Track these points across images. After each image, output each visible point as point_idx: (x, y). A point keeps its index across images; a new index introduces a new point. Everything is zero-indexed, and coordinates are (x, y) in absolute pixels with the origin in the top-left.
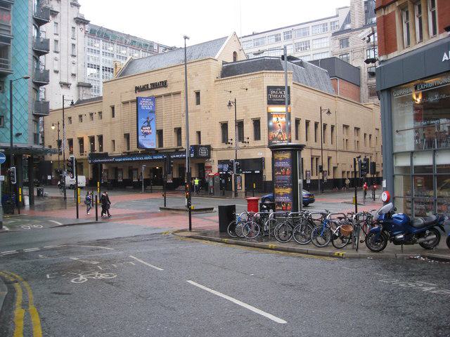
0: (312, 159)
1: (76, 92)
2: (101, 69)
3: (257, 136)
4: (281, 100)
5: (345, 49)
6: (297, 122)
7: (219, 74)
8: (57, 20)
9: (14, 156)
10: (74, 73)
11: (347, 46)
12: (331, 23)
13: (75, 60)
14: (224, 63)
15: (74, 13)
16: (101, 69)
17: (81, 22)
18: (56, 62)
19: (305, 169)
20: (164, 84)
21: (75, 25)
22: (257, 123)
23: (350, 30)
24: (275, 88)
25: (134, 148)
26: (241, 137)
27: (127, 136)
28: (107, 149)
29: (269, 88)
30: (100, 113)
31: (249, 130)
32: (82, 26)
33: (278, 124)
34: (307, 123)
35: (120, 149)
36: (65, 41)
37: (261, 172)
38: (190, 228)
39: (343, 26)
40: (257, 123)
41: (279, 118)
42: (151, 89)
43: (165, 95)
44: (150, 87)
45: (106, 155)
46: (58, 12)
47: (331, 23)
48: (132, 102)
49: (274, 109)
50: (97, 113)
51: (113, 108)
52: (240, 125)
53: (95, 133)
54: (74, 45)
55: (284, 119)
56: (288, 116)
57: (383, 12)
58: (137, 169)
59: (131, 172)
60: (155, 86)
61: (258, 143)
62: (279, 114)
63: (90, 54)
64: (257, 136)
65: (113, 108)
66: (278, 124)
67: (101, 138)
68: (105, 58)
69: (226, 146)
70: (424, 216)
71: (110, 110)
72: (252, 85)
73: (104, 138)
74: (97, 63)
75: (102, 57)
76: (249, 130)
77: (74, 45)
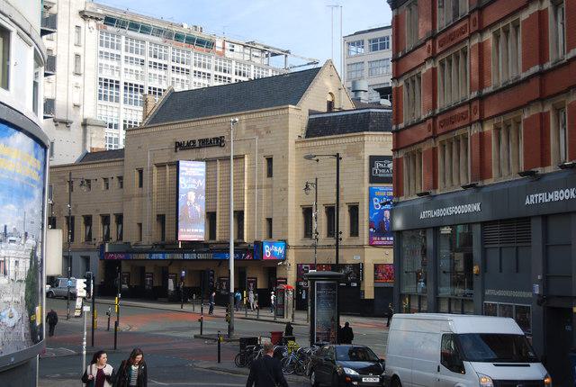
0: (371, 245)
1: (82, 130)
2: (122, 86)
3: (354, 232)
7: (303, 133)
10: (77, 103)
13: (79, 80)
14: (311, 113)
16: (122, 86)
20: (219, 142)
21: (81, 22)
26: (332, 230)
28: (131, 236)
29: (373, 159)
30: (120, 178)
37: (359, 285)
38: (115, 348)
42: (200, 147)
46: (54, 4)
50: (115, 178)
52: (332, 212)
53: (112, 211)
54: (77, 56)
57: (433, 142)
60: (205, 143)
61: (355, 241)
63: (104, 61)
64: (354, 232)
65: (141, 172)
67: (120, 219)
68: (129, 66)
69: (309, 242)
70: (140, 363)
71: (137, 175)
75: (124, 65)
77: (77, 56)
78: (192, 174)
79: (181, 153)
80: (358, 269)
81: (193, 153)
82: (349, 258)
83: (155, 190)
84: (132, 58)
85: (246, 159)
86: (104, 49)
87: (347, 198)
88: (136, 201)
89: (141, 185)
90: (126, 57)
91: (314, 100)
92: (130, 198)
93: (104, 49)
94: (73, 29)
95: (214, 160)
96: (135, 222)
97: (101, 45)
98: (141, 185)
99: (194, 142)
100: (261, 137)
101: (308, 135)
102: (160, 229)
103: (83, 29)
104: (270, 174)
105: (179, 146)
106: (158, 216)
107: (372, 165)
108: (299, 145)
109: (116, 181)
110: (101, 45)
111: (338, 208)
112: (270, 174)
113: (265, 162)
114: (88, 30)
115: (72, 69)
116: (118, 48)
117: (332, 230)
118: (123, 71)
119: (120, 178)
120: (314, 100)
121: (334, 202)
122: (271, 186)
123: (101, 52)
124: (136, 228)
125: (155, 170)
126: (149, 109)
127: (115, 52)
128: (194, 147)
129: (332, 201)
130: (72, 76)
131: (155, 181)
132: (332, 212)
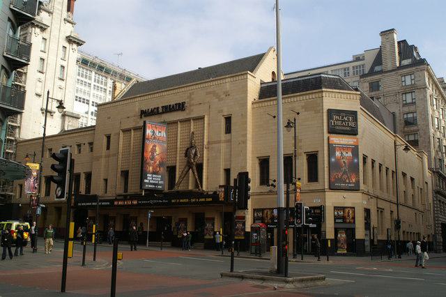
2: (91, 103)
3: (313, 176)
4: (344, 128)
5: (377, 92)
6: (365, 158)
8: (45, 35)
9: (4, 235)
11: (378, 90)
12: (353, 67)
13: (63, 84)
15: (68, 30)
16: (91, 103)
17: (74, 42)
18: (39, 84)
19: (372, 224)
20: (180, 107)
21: (67, 45)
22: (313, 159)
23: (381, 72)
24: (338, 112)
25: (133, 188)
26: (289, 178)
27: (125, 174)
28: (97, 189)
29: (331, 112)
30: (91, 144)
31: (301, 167)
32: (75, 46)
33: (342, 160)
34: (373, 162)
35: (115, 188)
36: (53, 62)
37: (319, 226)
39: (372, 68)
40: (313, 159)
41: (344, 153)
42: (163, 113)
43: (182, 121)
44: (160, 110)
45: (95, 198)
47: (353, 67)
48: (136, 129)
49: (337, 140)
51: (109, 137)
55: (350, 154)
56: (355, 150)
58: (135, 219)
59: (127, 221)
60: (168, 109)
61: (314, 186)
62: (344, 148)
63: (80, 87)
65: (109, 137)
66: (342, 160)
68: (96, 92)
69: (266, 189)
72: (306, 108)
73: (231, 172)
74: (86, 97)
75: (93, 91)
76: (301, 167)
78: (156, 133)
79: (148, 120)
80: (317, 214)
81: (156, 118)
82: (307, 202)
83: (121, 151)
84: (98, 87)
85: (206, 119)
86: (80, 78)
87: (307, 146)
88: (103, 161)
89: (108, 148)
90: (95, 86)
91: (264, 73)
92: (98, 158)
93: (80, 78)
94: (61, 48)
95: (175, 123)
96: (102, 177)
97: (79, 75)
98: (108, 148)
99: (158, 108)
100: (220, 99)
101: (260, 97)
102: (123, 184)
103: (68, 49)
104: (228, 130)
105: (144, 113)
106: (122, 172)
107: (330, 117)
108: (255, 106)
109: (87, 145)
110: (79, 75)
111: (295, 156)
112: (228, 130)
113: (223, 121)
114: (71, 51)
115: (58, 75)
116: (90, 79)
117: (289, 178)
118: (91, 95)
119: (91, 144)
120: (264, 73)
121: (97, 248)
122: (229, 141)
123: (78, 80)
124: (102, 183)
125: (121, 135)
126: (117, 92)
127: (87, 81)
128: (158, 113)
129: (290, 151)
130: (57, 80)
131: (121, 143)
132: (289, 161)
